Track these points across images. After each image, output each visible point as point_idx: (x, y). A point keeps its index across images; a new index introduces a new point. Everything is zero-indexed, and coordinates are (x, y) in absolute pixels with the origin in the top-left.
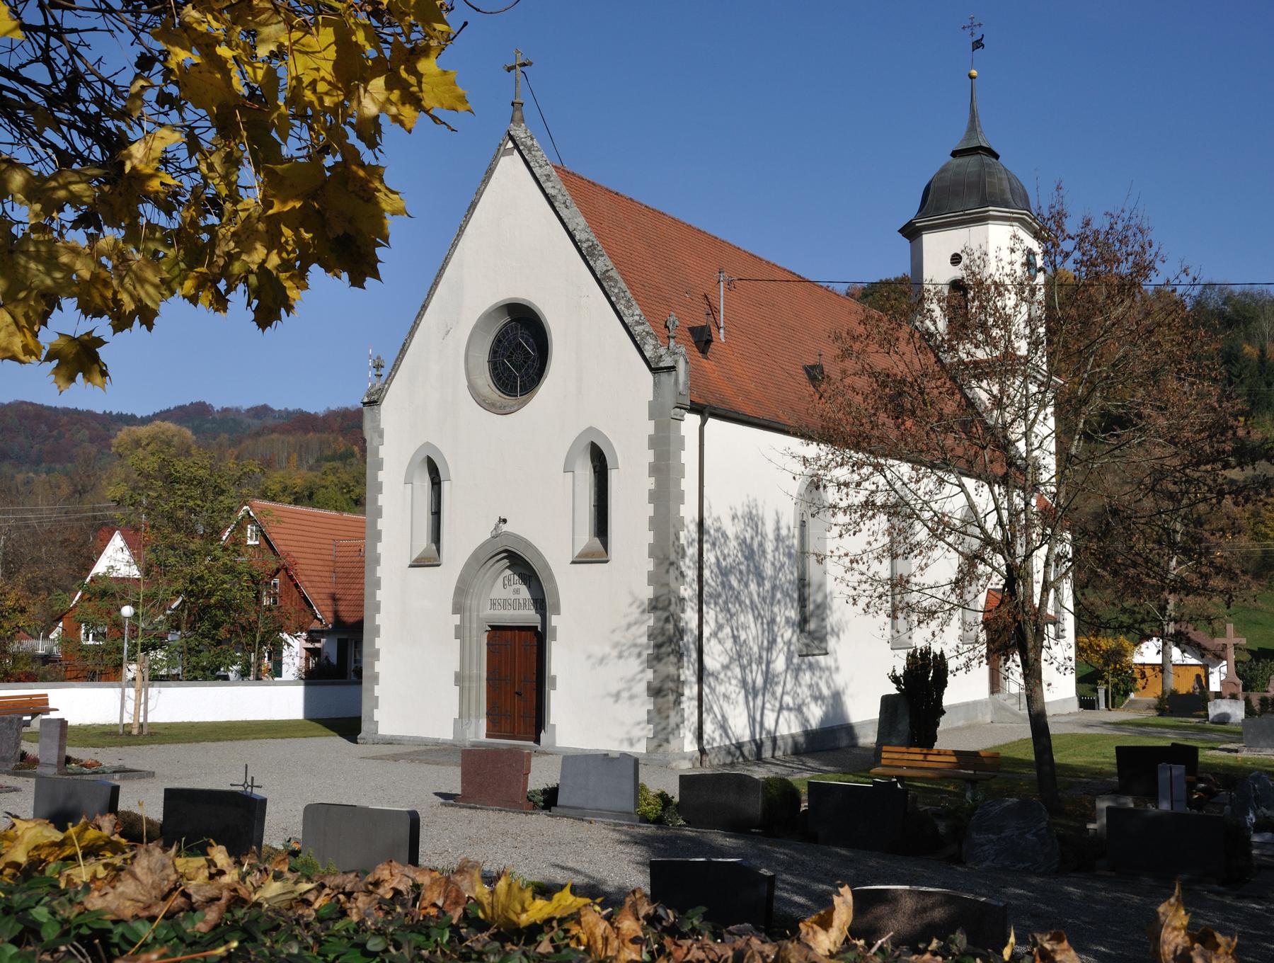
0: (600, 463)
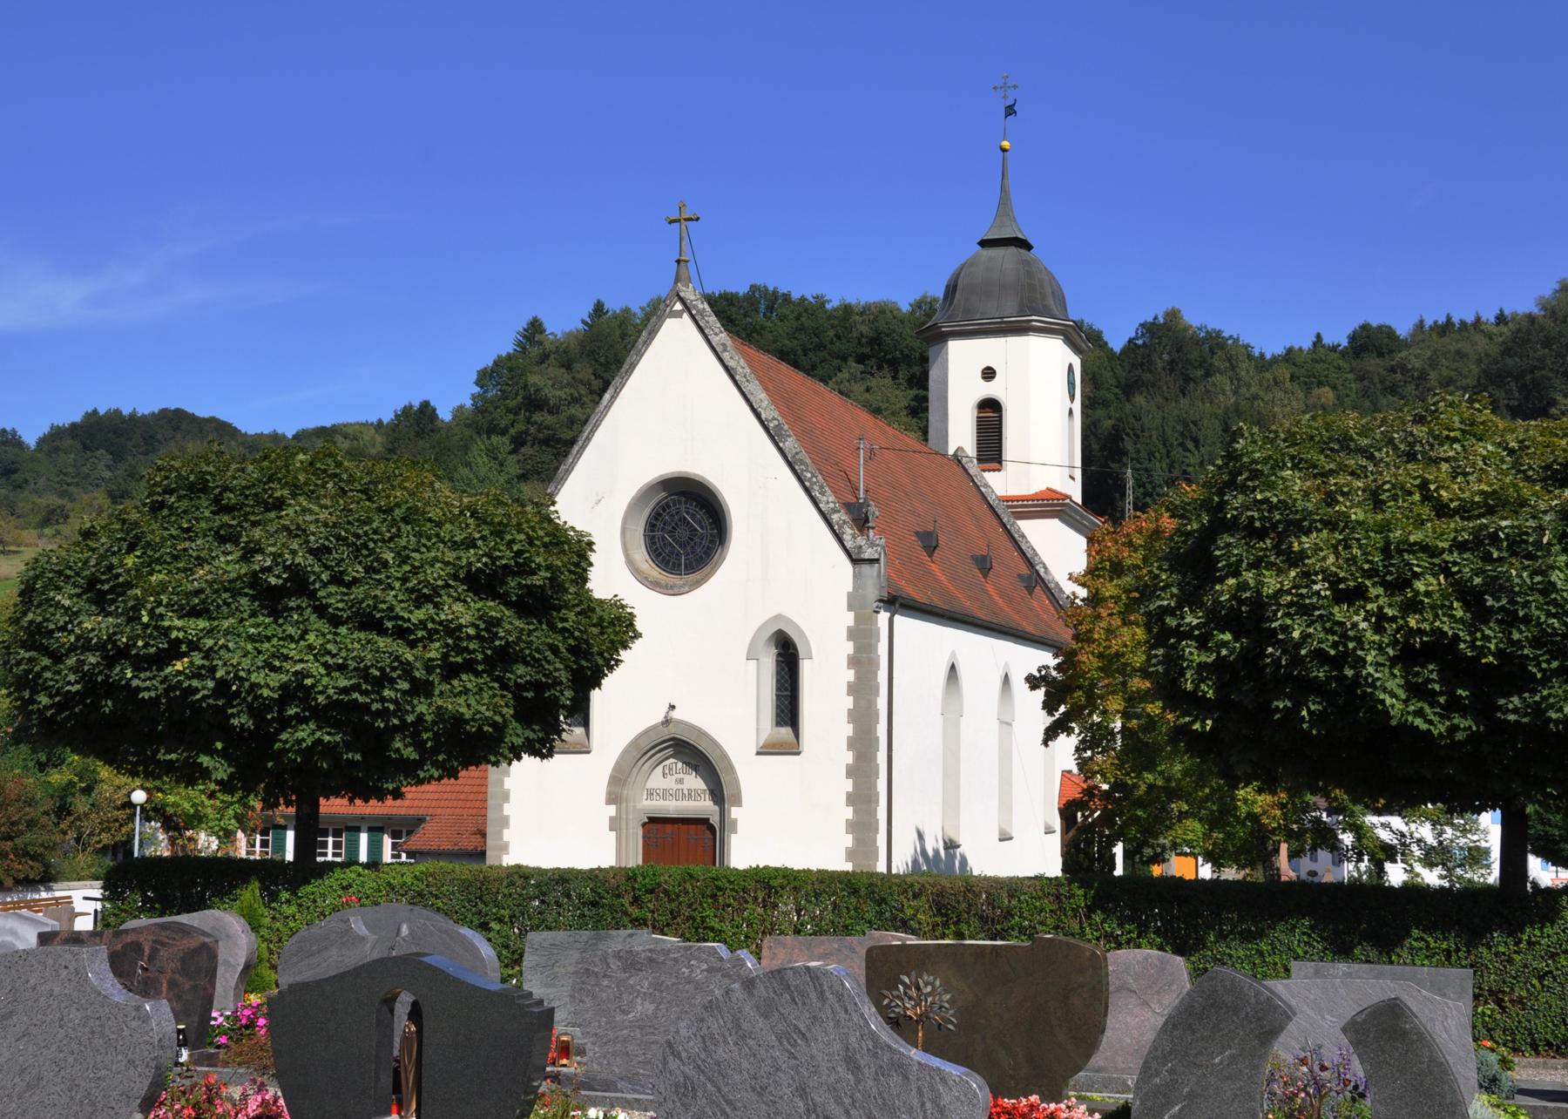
0: (787, 655)
